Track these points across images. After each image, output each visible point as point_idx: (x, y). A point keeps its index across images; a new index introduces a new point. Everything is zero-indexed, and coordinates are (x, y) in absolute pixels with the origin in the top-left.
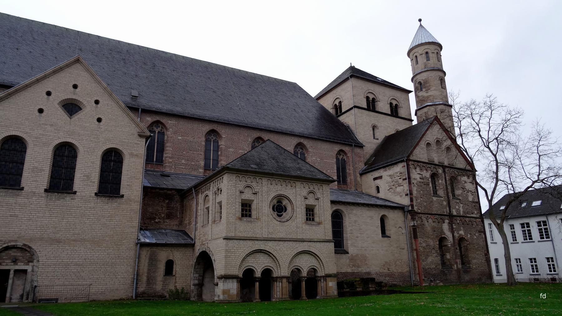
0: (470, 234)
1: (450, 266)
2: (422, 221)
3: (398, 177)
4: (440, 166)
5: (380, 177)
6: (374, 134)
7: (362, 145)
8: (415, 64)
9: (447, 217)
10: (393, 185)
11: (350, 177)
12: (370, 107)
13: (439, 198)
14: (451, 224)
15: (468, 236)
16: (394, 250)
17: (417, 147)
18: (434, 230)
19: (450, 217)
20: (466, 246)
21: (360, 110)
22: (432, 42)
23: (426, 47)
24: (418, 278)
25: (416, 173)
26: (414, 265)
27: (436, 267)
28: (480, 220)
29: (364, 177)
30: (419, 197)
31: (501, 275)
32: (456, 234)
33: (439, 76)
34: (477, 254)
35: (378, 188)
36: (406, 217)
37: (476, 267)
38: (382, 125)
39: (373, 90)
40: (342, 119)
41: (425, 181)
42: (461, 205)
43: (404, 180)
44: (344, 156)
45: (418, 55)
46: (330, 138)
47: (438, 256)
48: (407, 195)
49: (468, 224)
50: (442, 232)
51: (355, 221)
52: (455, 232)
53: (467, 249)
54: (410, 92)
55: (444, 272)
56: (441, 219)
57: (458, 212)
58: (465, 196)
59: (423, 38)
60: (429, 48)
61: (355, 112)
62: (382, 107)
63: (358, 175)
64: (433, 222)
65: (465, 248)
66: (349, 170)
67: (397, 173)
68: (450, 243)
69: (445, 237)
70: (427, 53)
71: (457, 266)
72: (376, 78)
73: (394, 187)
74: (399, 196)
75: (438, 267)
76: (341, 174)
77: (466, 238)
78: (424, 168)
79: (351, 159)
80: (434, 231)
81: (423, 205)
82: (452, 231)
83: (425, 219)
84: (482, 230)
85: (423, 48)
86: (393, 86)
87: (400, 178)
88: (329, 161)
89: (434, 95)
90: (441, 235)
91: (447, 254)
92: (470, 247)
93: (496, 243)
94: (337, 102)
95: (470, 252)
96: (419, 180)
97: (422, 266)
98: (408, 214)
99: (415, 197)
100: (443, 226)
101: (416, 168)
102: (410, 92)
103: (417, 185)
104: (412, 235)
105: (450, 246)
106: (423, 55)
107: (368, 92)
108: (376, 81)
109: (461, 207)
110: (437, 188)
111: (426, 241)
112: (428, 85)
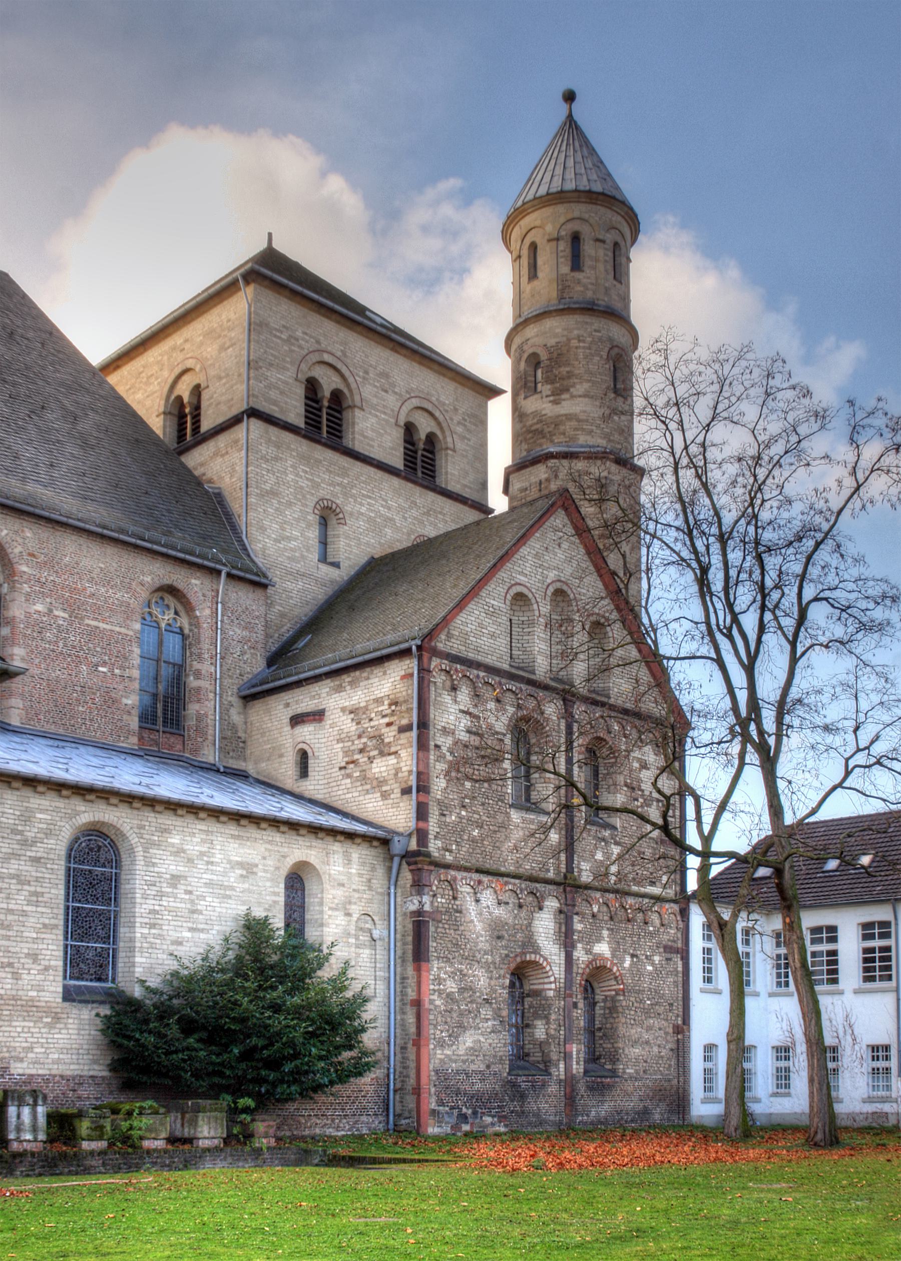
0: (633, 956)
1: (541, 1066)
2: (455, 898)
3: (384, 716)
6: (324, 543)
7: (264, 581)
8: (525, 278)
10: (361, 751)
14: (565, 917)
15: (624, 961)
18: (497, 931)
20: (614, 1000)
21: (274, 431)
25: (453, 708)
27: (488, 1067)
28: (676, 907)
29: (258, 709)
32: (580, 955)
35: (304, 760)
36: (393, 879)
37: (637, 1072)
38: (363, 510)
39: (339, 354)
40: (195, 459)
43: (403, 729)
44: (182, 613)
46: (122, 531)
48: (406, 791)
50: (530, 943)
51: (175, 880)
52: (579, 945)
53: (613, 1009)
54: (494, 392)
59: (570, 174)
60: (586, 216)
61: (251, 436)
62: (370, 433)
63: (235, 700)
64: (499, 903)
65: (608, 1004)
67: (378, 701)
68: (553, 986)
69: (535, 963)
71: (568, 1068)
72: (362, 310)
73: (362, 759)
74: (379, 794)
77: (615, 969)
78: (487, 693)
80: (499, 938)
82: (567, 939)
84: (680, 945)
87: (389, 725)
88: (105, 626)
89: (583, 416)
90: (525, 954)
94: (184, 390)
95: (623, 1020)
98: (405, 866)
99: (439, 802)
100: (536, 923)
101: (454, 689)
102: (494, 392)
103: (451, 753)
105: (551, 993)
107: (315, 358)
111: (461, 971)
112: (564, 370)
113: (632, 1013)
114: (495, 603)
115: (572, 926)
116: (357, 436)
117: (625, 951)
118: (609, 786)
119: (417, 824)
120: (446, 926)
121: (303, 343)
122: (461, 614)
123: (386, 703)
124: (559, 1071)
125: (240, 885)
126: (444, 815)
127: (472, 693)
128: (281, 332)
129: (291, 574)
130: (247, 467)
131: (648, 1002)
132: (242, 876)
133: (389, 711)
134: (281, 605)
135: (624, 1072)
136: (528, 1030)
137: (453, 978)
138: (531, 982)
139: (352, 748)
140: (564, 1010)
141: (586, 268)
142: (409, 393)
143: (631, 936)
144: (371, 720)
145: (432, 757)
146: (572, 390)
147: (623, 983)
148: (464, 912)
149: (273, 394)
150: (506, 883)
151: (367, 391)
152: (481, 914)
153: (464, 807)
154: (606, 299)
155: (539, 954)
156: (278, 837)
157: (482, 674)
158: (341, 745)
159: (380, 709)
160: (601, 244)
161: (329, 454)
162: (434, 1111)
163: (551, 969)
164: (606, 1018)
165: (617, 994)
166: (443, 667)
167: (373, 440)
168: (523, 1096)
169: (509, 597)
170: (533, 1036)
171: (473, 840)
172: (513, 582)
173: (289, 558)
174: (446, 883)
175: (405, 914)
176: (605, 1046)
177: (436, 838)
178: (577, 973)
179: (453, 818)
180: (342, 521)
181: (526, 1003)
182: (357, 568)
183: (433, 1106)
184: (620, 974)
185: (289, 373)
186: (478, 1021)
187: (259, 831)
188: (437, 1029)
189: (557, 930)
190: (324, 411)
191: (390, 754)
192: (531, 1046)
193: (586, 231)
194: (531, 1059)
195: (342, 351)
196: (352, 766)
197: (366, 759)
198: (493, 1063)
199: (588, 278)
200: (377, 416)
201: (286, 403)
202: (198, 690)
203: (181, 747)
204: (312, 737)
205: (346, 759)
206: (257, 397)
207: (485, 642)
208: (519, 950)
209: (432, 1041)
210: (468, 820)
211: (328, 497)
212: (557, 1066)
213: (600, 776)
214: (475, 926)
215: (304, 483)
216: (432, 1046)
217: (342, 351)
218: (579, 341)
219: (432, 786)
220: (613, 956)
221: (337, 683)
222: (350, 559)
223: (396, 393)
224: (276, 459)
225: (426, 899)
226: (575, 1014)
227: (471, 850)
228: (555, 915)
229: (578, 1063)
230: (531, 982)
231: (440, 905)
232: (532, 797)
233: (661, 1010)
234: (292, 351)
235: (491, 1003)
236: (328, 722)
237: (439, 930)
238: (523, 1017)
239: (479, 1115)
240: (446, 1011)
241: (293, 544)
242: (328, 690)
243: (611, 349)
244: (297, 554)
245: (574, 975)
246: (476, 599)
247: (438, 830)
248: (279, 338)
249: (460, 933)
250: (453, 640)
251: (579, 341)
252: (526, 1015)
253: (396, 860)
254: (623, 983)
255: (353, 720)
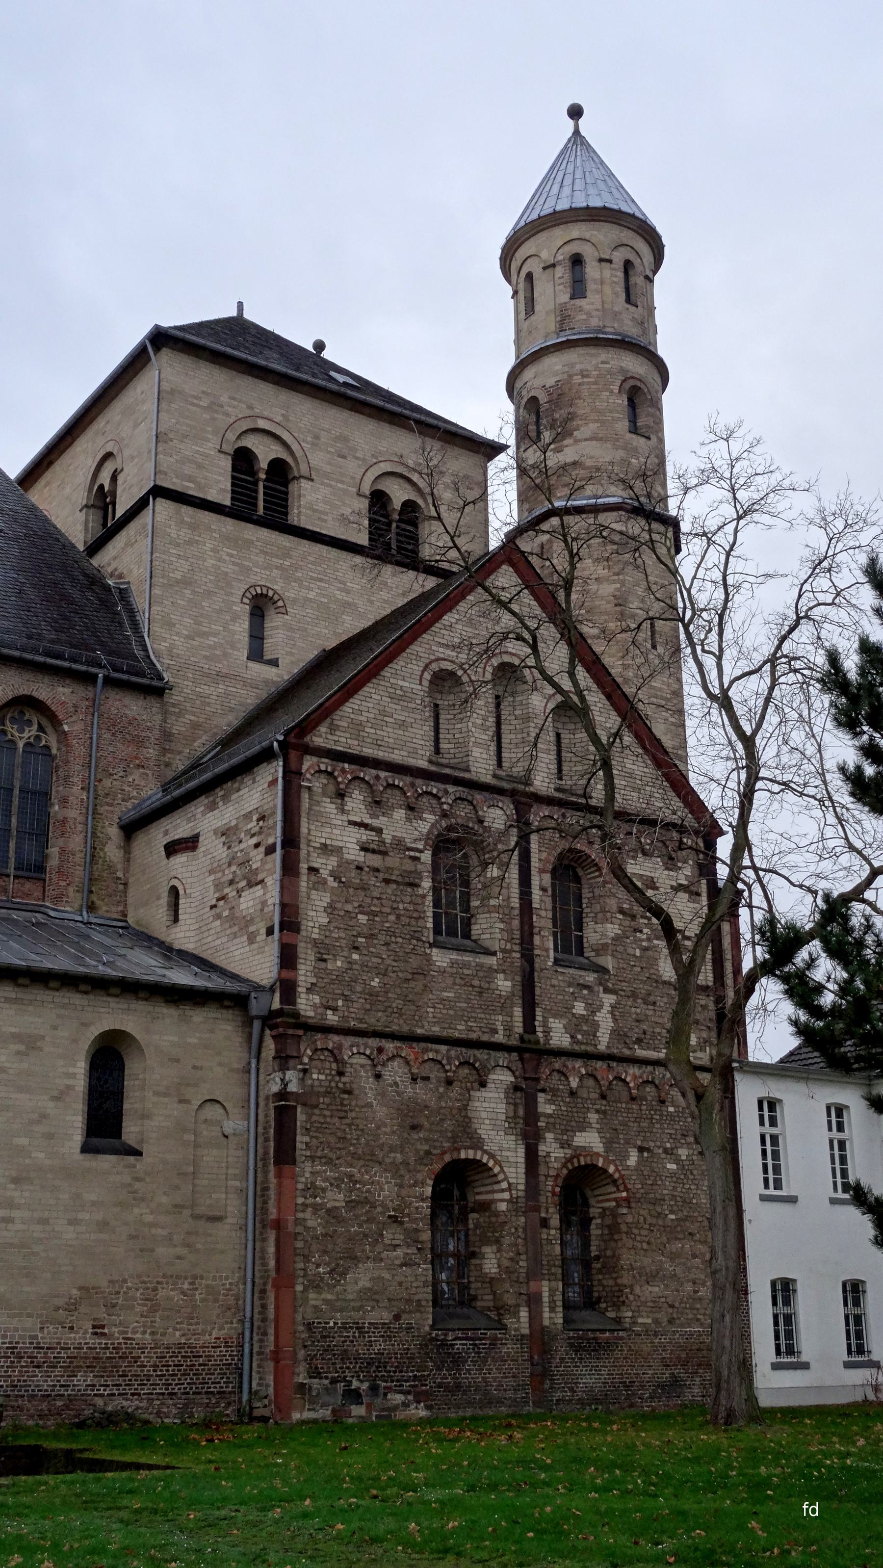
0: (641, 1149)
1: (493, 1315)
3: (253, 836)
4: (501, 792)
5: (190, 844)
8: (522, 315)
9: (502, 1058)
10: (231, 882)
11: (61, 842)
12: (255, 505)
13: (467, 958)
15: (626, 1157)
16: (152, 1225)
17: (367, 689)
19: (521, 1059)
20: (614, 1215)
21: (187, 511)
22: (605, 208)
23: (576, 230)
24: (270, 1379)
25: (339, 820)
26: (264, 1307)
30: (343, 943)
31: (805, 1366)
33: (622, 370)
34: (673, 1256)
37: (656, 1321)
38: (311, 595)
39: (278, 419)
41: (393, 861)
42: (609, 1000)
44: (49, 729)
45: (537, 271)
47: (417, 1258)
49: (633, 1099)
52: (549, 1136)
54: (493, 449)
55: (444, 1344)
56: (465, 1063)
57: (585, 1033)
58: (638, 952)
60: (587, 236)
61: (158, 518)
62: (321, 506)
63: (114, 832)
65: (608, 1221)
66: (64, 801)
67: (248, 816)
68: (506, 1195)
70: (577, 261)
75: (412, 1319)
76: (14, 820)
77: (611, 1169)
79: (79, 749)
80: (414, 1127)
81: (359, 988)
83: (363, 1060)
85: (560, 234)
86: (435, 422)
90: (458, 1150)
91: (488, 1251)
92: (629, 1219)
93: (792, 1200)
95: (630, 1243)
96: (353, 853)
97: (303, 1314)
101: (341, 795)
104: (272, 1144)
105: (503, 1207)
106: (559, 271)
108: (322, 383)
109: (607, 1008)
110: (475, 903)
111: (351, 1176)
113: (644, 1232)
114: (406, 684)
115: (536, 1108)
116: (303, 510)
117: (627, 1142)
118: (596, 914)
119: (279, 973)
120: (327, 1113)
121: (230, 409)
122: (351, 700)
123: (255, 818)
124: (519, 1321)
125: (15, 1065)
126: (325, 960)
127: (370, 800)
128: (200, 399)
129: (208, 675)
130: (152, 554)
131: (673, 1217)
132: (18, 1053)
133: (257, 829)
134: (193, 714)
135: (635, 1323)
136: (474, 1261)
137: (338, 1187)
138: (476, 1190)
139: (223, 880)
140: (525, 1229)
141: (588, 293)
142: (376, 458)
143: (638, 1120)
144: (240, 842)
145: (304, 884)
146: (575, 433)
147: (627, 1189)
148: (356, 1092)
149: (188, 470)
150: (425, 1051)
151: (318, 459)
152: (383, 1094)
153: (356, 948)
154: (616, 325)
155: (481, 1149)
156: (77, 999)
157: (383, 774)
158: (212, 877)
159: (249, 826)
160: (607, 265)
161: (264, 534)
162: (303, 1385)
163: (502, 1171)
164: (604, 1241)
165: (618, 1206)
166: (323, 767)
167: (326, 514)
168: (457, 1361)
169: (427, 676)
170: (481, 1269)
171: (372, 994)
172: (433, 657)
173: (205, 657)
174: (326, 1053)
175: (267, 1098)
176: (605, 1282)
177: (309, 990)
178: (547, 1176)
179: (339, 963)
180: (283, 610)
181: (470, 1221)
182: (302, 665)
183: (302, 1379)
184: (622, 1177)
185: (209, 444)
186: (379, 1248)
187: (47, 992)
188: (309, 1261)
189: (511, 1114)
190: (261, 484)
191: (257, 884)
192: (479, 1285)
193: (589, 253)
194: (479, 1304)
195: (283, 415)
196: (221, 903)
197: (234, 893)
198: (404, 1312)
199: (592, 304)
200: (330, 486)
201: (205, 478)
202: (64, 821)
203: (40, 894)
204: (184, 870)
205: (217, 895)
206: (166, 474)
207: (389, 734)
208: (446, 1145)
209: (301, 1280)
210: (362, 965)
211: (262, 583)
212: (516, 1314)
213: (585, 901)
214: (374, 1112)
215: (229, 569)
216: (299, 1288)
217: (283, 415)
218: (583, 376)
219: (304, 922)
220: (608, 1149)
221: (211, 799)
222: (292, 654)
223: (357, 458)
224: (190, 543)
225: (290, 1075)
226: (544, 1236)
227: (368, 1007)
228: (506, 1093)
229: (552, 1309)
230: (476, 1190)
231: (316, 1083)
232: (473, 932)
233: (693, 1228)
234: (214, 419)
235: (402, 1223)
236: (201, 849)
237: (314, 1118)
238: (467, 1242)
239: (382, 1391)
240: (325, 1235)
241: (212, 640)
242: (202, 808)
243: (624, 381)
244: (218, 652)
245: (542, 1178)
246: (374, 681)
247: (314, 981)
248: (198, 406)
249: (348, 1121)
250: (337, 733)
251: (583, 376)
252: (472, 1238)
253: (257, 1024)
254: (627, 1189)
255: (224, 844)
